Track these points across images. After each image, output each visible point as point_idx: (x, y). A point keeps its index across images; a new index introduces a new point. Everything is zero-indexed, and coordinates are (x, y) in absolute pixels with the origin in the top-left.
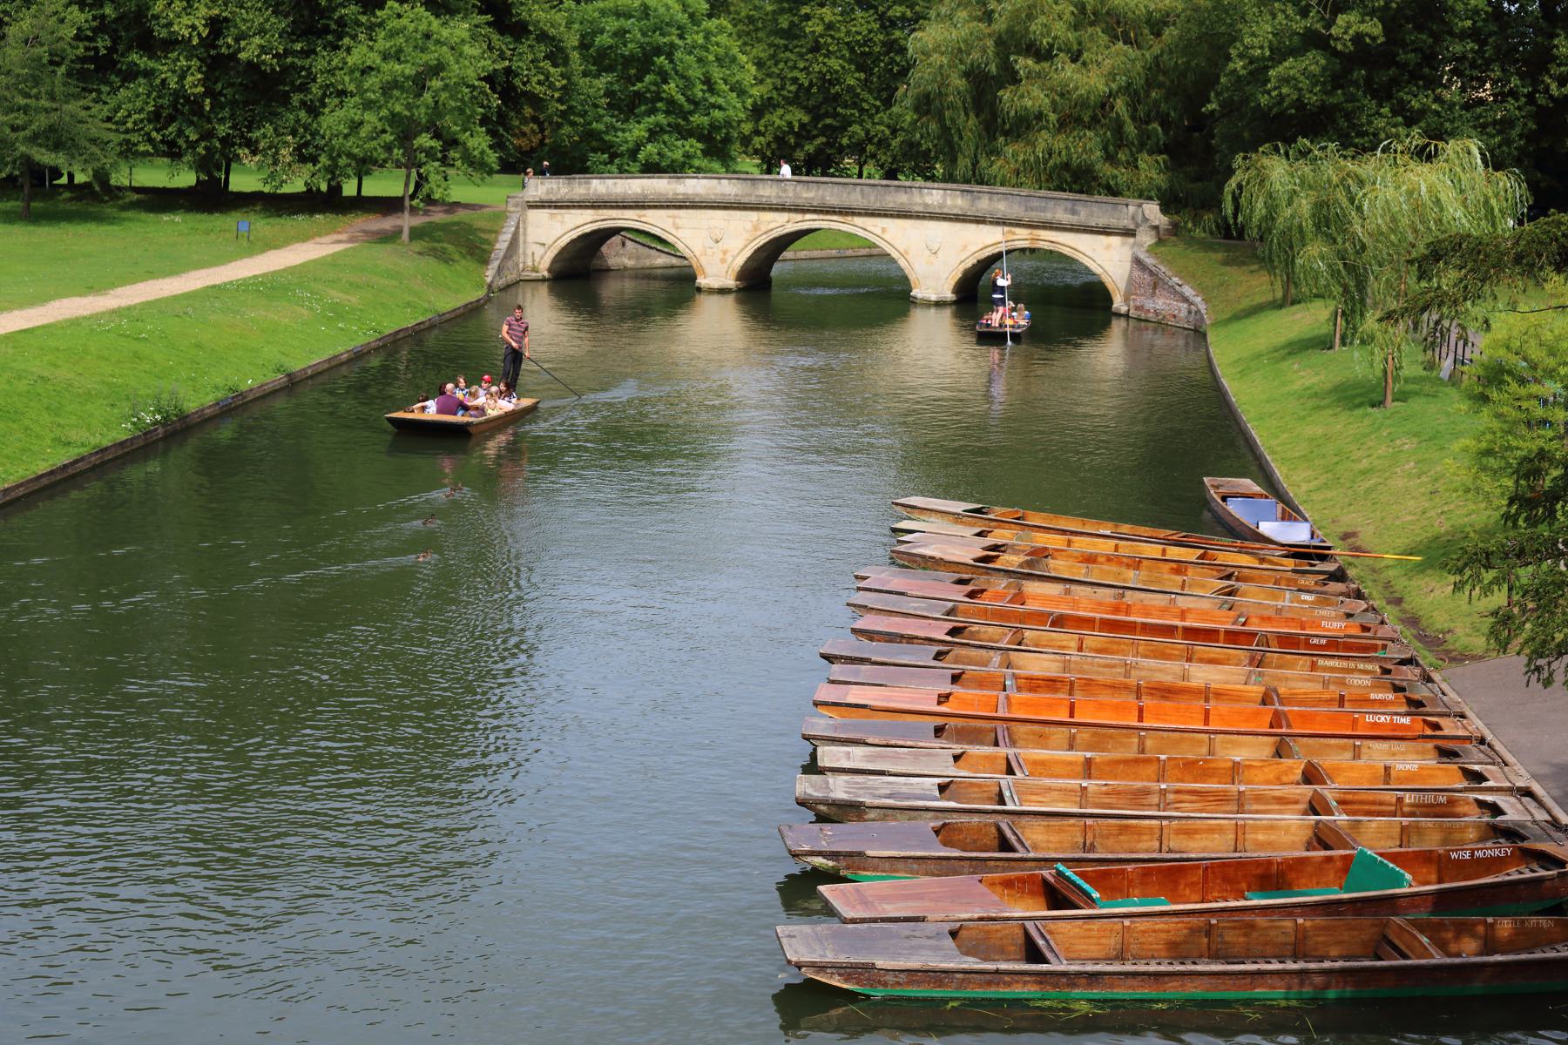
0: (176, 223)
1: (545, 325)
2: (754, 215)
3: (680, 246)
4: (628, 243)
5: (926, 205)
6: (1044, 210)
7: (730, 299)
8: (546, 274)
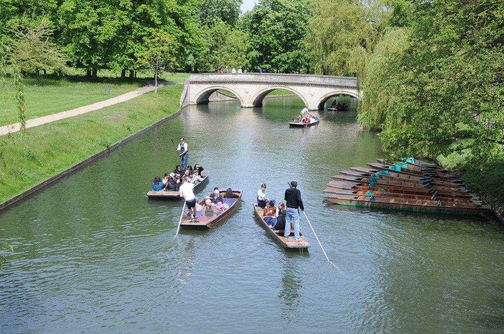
0: (80, 85)
1: (194, 116)
2: (258, 86)
3: (236, 94)
4: (218, 94)
5: (310, 81)
6: (345, 82)
7: (252, 109)
8: (196, 103)
